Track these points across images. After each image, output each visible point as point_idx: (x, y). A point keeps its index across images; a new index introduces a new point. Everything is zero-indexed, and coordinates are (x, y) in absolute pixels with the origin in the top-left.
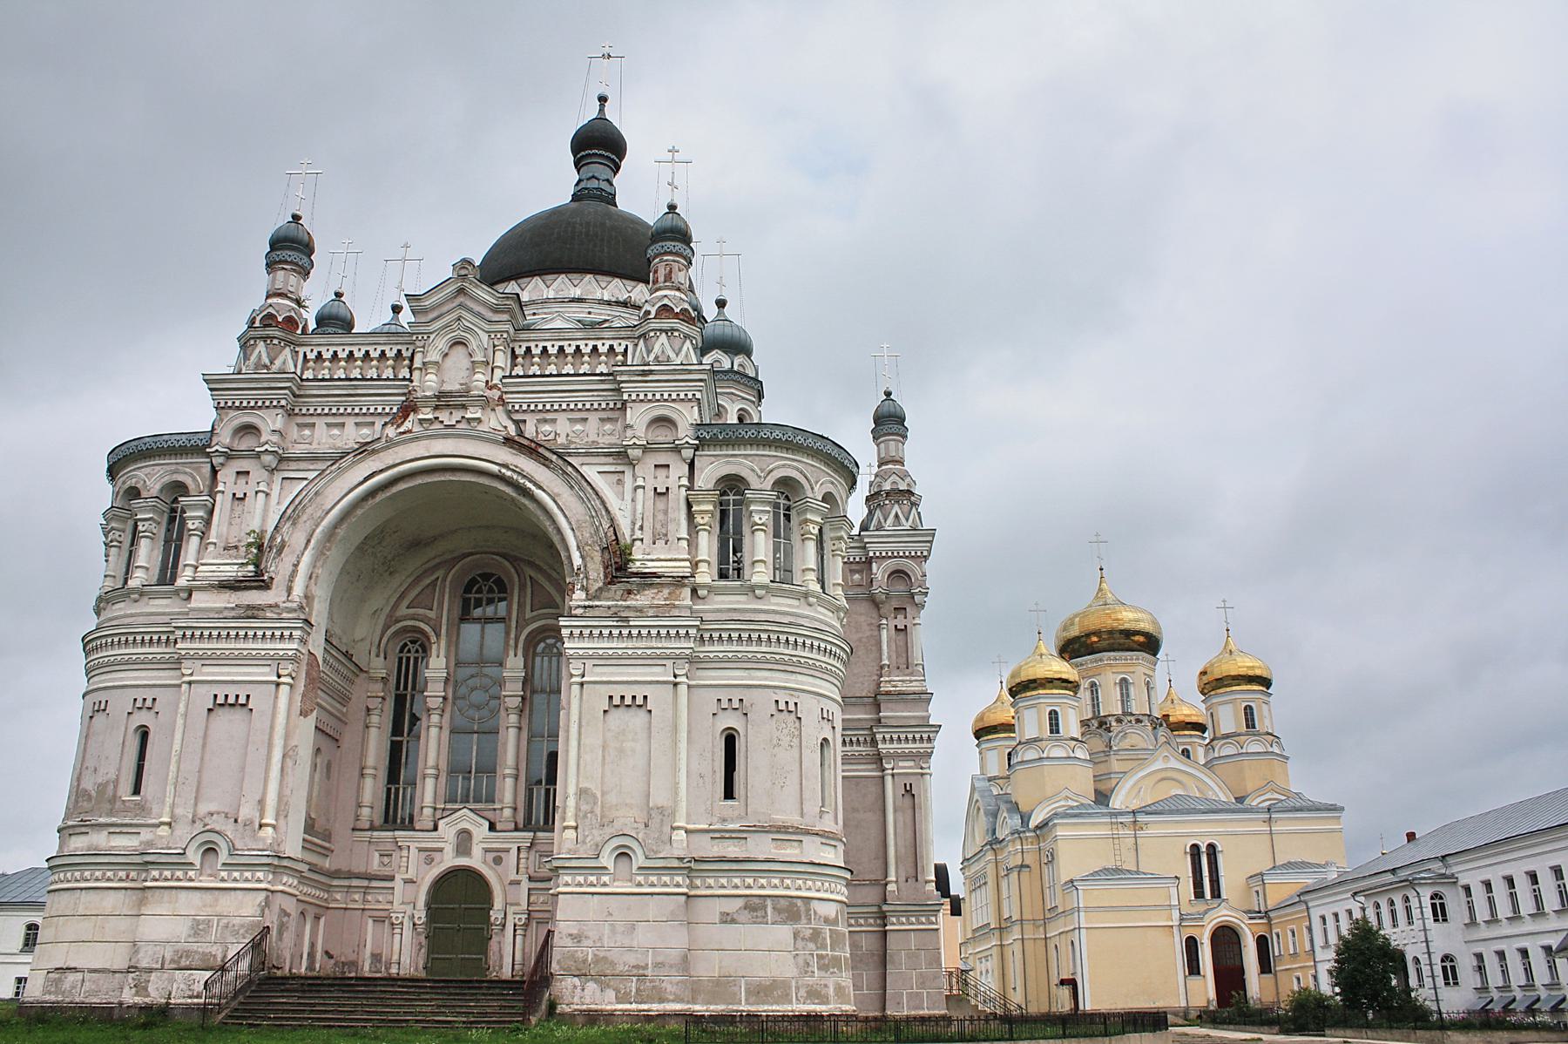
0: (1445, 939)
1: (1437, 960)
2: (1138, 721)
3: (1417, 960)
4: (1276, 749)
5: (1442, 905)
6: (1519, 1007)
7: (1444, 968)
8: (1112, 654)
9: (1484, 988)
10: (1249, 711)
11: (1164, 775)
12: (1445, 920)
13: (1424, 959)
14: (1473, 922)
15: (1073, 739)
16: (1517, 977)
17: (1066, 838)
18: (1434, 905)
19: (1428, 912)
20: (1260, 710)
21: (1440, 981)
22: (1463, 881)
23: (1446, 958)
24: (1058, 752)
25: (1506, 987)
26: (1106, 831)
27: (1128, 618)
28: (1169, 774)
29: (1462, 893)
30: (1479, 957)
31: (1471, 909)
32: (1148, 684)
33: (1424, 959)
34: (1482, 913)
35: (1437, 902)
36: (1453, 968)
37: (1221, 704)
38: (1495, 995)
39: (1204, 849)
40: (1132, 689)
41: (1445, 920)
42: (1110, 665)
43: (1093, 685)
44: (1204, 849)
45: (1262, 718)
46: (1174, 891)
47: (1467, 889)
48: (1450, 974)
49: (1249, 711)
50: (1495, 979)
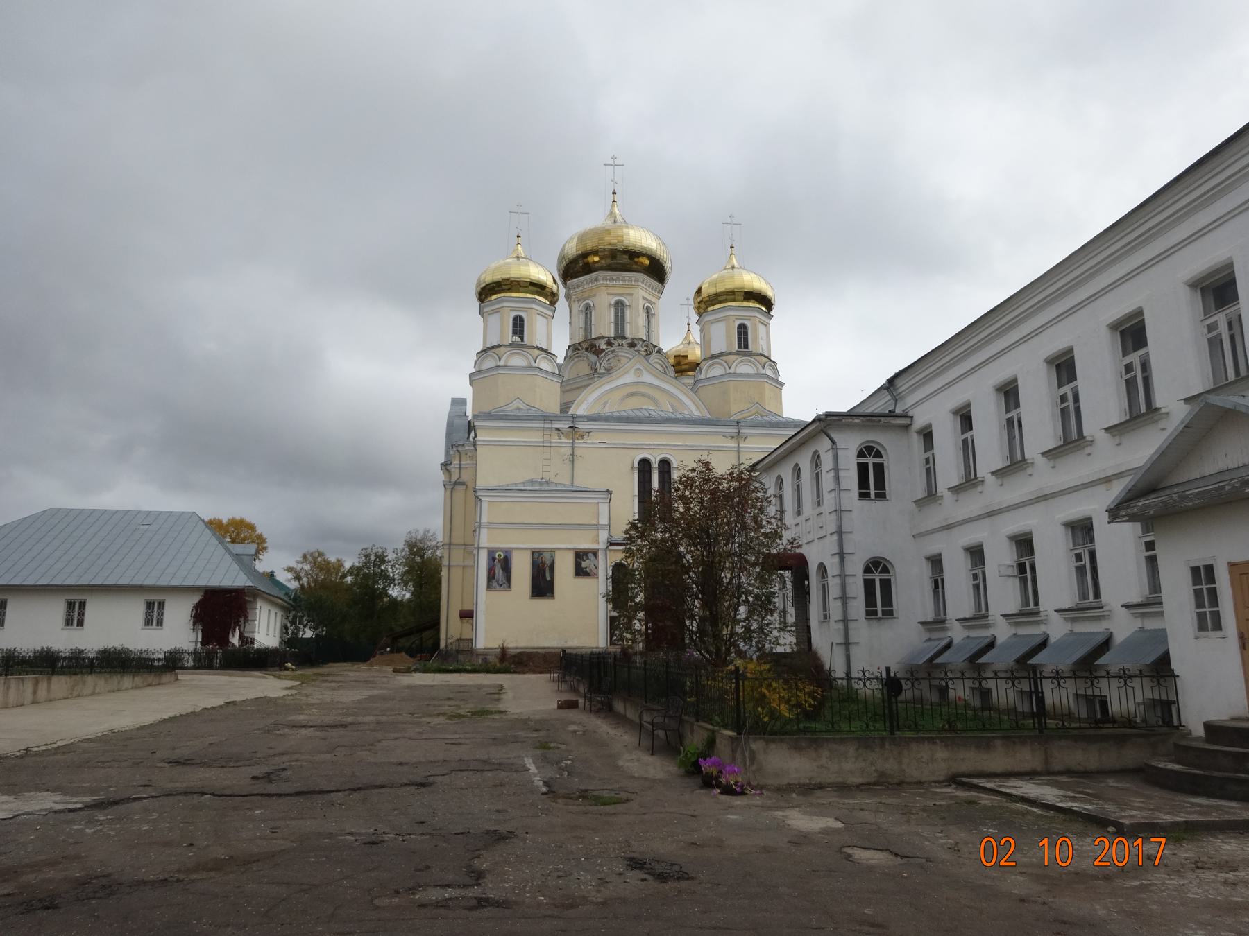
0: (877, 529)
1: (856, 567)
2: (632, 345)
3: (822, 568)
4: (769, 373)
5: (879, 469)
6: (1000, 660)
7: (869, 585)
8: (609, 273)
9: (938, 623)
10: (743, 331)
11: (633, 389)
12: (881, 495)
13: (833, 568)
14: (932, 495)
15: (538, 348)
16: (1004, 596)
17: (488, 444)
18: (862, 469)
19: (850, 478)
20: (756, 330)
21: (858, 606)
22: (919, 423)
23: (876, 565)
24: (517, 361)
25: (980, 618)
26: (536, 438)
27: (640, 238)
28: (641, 389)
29: (917, 442)
30: (936, 562)
31: (930, 473)
32: (648, 310)
33: (833, 568)
34: (949, 472)
35: (870, 461)
36: (886, 585)
37: (712, 322)
38: (957, 633)
39: (655, 464)
40: (628, 313)
41: (881, 495)
42: (606, 286)
43: (588, 308)
44: (655, 464)
45: (756, 338)
46: (604, 508)
47: (927, 436)
48: (879, 592)
49: (743, 331)
50: (959, 602)
